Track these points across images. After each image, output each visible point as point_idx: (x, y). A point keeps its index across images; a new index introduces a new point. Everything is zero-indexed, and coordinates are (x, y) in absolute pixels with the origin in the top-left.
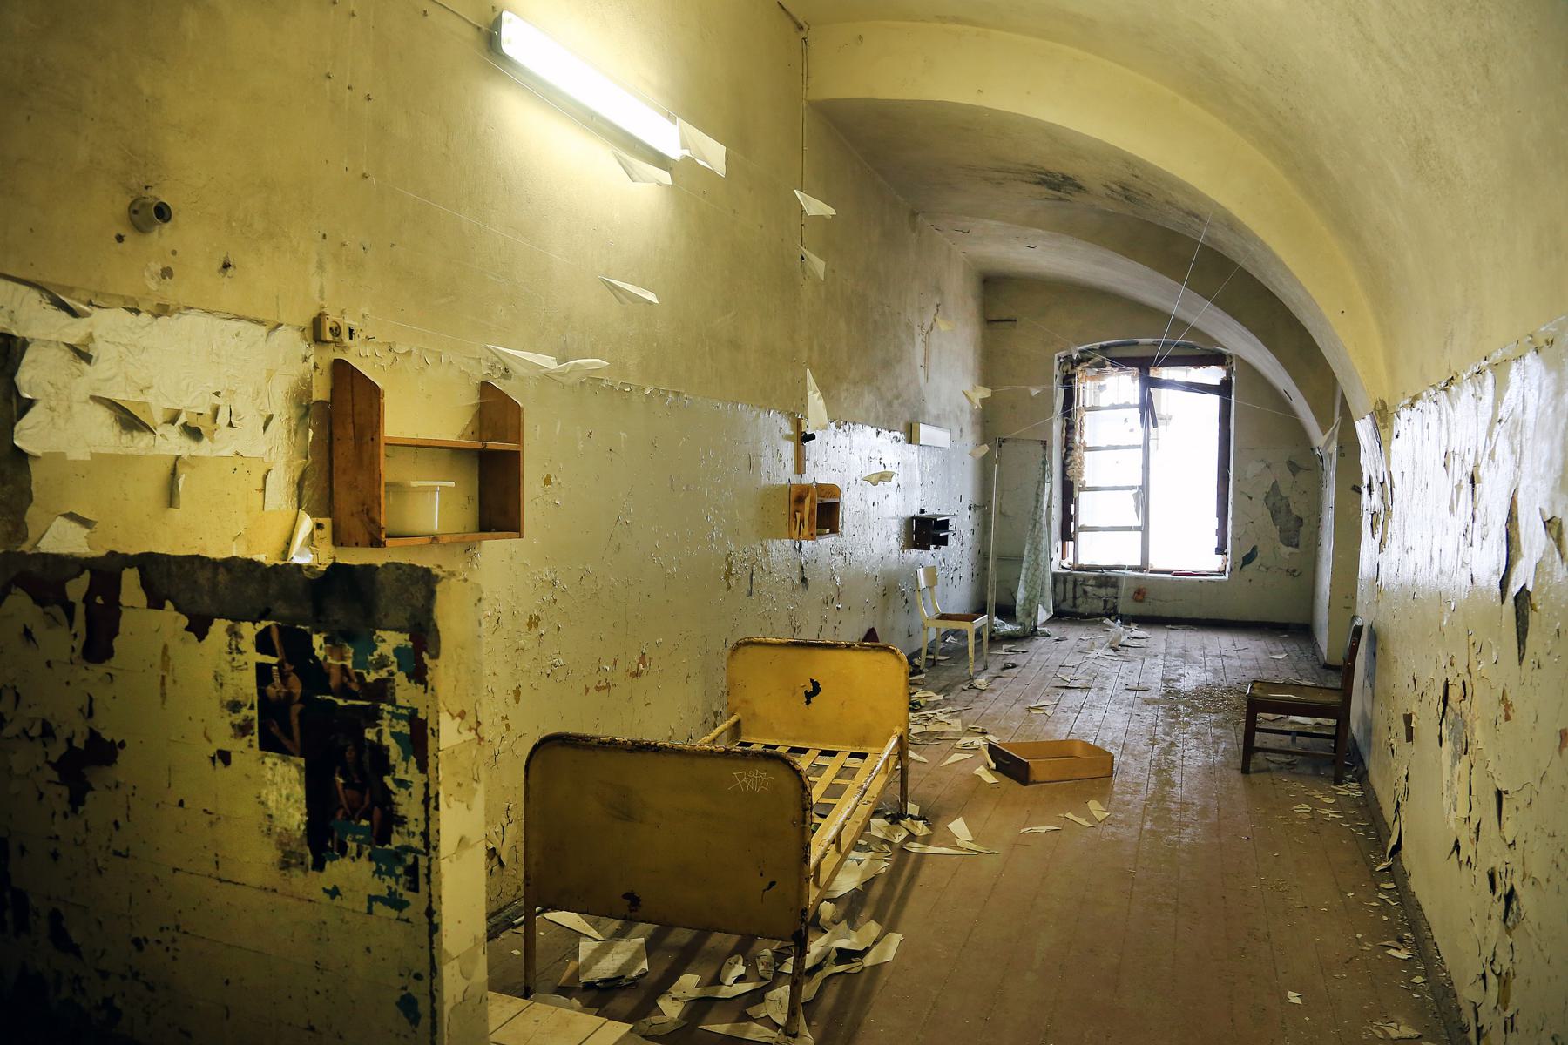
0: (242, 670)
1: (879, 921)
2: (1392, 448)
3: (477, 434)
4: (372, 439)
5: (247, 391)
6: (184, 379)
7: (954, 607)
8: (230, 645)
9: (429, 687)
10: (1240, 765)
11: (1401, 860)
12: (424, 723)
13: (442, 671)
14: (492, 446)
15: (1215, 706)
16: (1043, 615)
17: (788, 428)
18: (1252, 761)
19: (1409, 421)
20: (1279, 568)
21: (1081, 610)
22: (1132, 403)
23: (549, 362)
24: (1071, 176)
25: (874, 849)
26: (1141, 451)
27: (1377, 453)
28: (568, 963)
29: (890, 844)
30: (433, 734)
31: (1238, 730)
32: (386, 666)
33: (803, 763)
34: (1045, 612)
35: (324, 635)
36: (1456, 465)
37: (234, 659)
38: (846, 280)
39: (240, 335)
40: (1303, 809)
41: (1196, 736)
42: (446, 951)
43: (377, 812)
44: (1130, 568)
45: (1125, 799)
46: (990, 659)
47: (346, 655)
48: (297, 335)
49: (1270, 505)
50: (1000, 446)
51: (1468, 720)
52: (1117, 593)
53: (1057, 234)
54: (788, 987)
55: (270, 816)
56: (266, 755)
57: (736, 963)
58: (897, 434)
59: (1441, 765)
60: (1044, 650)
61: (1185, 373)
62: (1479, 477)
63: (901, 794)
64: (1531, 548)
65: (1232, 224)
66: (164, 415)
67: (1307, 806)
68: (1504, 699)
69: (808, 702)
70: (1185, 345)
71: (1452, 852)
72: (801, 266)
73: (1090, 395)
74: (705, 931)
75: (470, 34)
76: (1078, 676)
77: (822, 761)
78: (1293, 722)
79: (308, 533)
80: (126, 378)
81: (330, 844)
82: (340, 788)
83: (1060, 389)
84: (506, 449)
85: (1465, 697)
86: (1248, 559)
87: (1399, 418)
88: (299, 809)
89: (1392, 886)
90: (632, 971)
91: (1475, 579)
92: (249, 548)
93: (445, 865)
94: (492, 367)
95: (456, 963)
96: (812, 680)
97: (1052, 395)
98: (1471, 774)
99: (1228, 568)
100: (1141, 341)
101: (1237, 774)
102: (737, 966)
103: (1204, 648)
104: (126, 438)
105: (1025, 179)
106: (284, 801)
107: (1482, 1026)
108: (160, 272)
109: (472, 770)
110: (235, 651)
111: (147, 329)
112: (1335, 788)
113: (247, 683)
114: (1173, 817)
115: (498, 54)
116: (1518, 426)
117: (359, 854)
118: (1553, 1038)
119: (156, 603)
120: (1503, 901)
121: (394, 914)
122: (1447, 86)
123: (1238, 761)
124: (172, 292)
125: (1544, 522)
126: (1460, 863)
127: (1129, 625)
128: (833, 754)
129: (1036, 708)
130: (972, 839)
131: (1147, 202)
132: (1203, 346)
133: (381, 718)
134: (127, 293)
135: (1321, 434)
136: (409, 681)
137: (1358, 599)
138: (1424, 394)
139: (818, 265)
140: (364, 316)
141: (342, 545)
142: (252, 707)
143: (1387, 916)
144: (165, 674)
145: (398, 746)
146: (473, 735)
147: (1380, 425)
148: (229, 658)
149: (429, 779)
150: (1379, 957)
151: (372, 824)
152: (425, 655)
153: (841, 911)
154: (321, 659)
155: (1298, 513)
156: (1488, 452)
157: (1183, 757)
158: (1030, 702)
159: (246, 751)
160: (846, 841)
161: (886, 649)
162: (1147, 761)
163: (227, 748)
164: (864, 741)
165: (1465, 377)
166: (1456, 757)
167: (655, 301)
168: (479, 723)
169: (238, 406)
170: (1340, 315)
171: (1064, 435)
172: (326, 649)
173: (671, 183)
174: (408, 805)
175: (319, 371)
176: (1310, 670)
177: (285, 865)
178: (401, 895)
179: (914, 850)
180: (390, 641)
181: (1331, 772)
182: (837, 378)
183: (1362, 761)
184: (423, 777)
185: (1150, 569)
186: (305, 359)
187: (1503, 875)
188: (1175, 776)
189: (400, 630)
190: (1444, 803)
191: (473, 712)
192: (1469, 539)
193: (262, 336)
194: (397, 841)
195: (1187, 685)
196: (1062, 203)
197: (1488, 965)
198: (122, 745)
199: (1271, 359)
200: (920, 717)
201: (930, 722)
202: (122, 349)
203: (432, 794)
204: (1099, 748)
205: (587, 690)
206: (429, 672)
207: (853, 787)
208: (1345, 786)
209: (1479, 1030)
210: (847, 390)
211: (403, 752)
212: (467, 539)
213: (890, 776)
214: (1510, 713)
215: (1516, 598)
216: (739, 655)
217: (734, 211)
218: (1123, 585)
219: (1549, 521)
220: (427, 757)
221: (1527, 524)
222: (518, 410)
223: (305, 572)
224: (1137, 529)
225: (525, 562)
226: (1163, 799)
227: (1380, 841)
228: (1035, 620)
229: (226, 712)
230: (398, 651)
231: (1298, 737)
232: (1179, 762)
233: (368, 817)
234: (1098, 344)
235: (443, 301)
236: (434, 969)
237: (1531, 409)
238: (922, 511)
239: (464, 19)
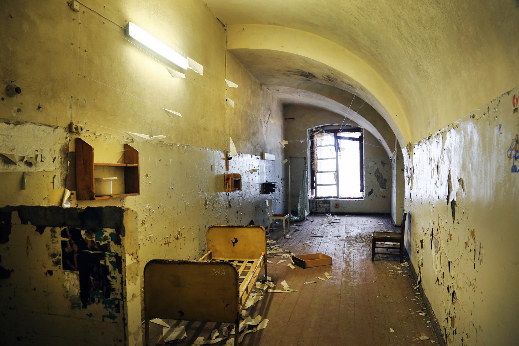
0: (56, 243)
1: (261, 315)
2: (413, 157)
3: (123, 161)
4: (90, 164)
5: (47, 149)
6: (26, 146)
7: (278, 212)
8: (52, 235)
9: (122, 246)
10: (371, 259)
11: (421, 286)
12: (121, 257)
13: (126, 241)
14: (129, 165)
15: (362, 240)
16: (306, 214)
17: (223, 156)
18: (375, 257)
19: (418, 149)
20: (380, 196)
21: (318, 211)
22: (332, 144)
23: (147, 137)
24: (311, 73)
25: (257, 292)
26: (335, 159)
27: (409, 159)
28: (160, 336)
29: (262, 290)
30: (124, 261)
31: (370, 247)
32: (107, 240)
33: (235, 264)
34: (307, 213)
35: (85, 231)
36: (432, 163)
37: (53, 240)
38: (240, 107)
39: (45, 131)
40: (391, 271)
41: (357, 250)
42: (129, 332)
43: (105, 288)
44: (333, 197)
45: (336, 271)
46: (290, 229)
47: (93, 237)
48: (63, 130)
49: (376, 176)
50: (291, 159)
51: (439, 241)
52: (330, 206)
53: (307, 91)
54: (233, 339)
55: (67, 291)
56: (66, 271)
57: (216, 332)
58: (258, 156)
59: (432, 255)
60: (307, 225)
61: (348, 134)
62: (439, 166)
63: (265, 274)
64: (455, 188)
65: (362, 89)
66: (19, 158)
67: (392, 270)
68: (449, 234)
69: (234, 245)
70: (348, 125)
71: (436, 282)
72: (226, 103)
73: (319, 142)
74: (204, 322)
75: (118, 29)
76: (319, 233)
77: (239, 264)
78: (386, 244)
79: (69, 197)
80: (6, 146)
81: (88, 299)
82: (92, 280)
83: (309, 141)
84: (134, 166)
85: (438, 234)
86: (370, 193)
87: (415, 148)
88: (77, 288)
89: (419, 293)
90: (181, 337)
91: (439, 198)
92: (49, 202)
93: (128, 303)
94: (128, 139)
95: (132, 336)
96: (235, 238)
97: (307, 143)
98: (441, 257)
99: (364, 196)
100: (334, 124)
101: (370, 262)
102: (216, 333)
103: (358, 222)
104: (6, 167)
105: (297, 74)
106: (72, 286)
107: (447, 334)
108: (17, 110)
109: (136, 272)
110: (54, 237)
111: (13, 129)
112: (401, 264)
113: (59, 247)
114: (352, 276)
115: (128, 36)
116: (449, 151)
117: (99, 302)
118: (467, 334)
119: (24, 222)
120: (452, 295)
121: (111, 321)
122: (425, 49)
123: (370, 257)
124: (22, 117)
125: (458, 180)
126: (439, 285)
127: (334, 216)
128: (242, 262)
129: (306, 244)
130: (289, 287)
131: (336, 81)
132: (353, 126)
133: (106, 257)
134: (6, 117)
135: (391, 153)
136: (115, 244)
137: (405, 205)
138: (422, 141)
139: (232, 103)
140: (85, 123)
141: (80, 200)
142: (60, 255)
143: (418, 303)
144: (28, 246)
145: (112, 266)
146: (136, 261)
147: (409, 150)
148: (52, 240)
149: (122, 276)
150: (416, 316)
151: (103, 292)
152: (120, 236)
153: (248, 313)
154: (84, 238)
155: (385, 178)
156: (441, 159)
157: (353, 257)
158: (304, 242)
159: (58, 271)
160: (249, 290)
161: (258, 227)
162: (342, 259)
163: (51, 269)
164: (252, 257)
165: (434, 136)
166: (436, 252)
167: (181, 116)
168: (137, 257)
169: (44, 155)
170: (396, 117)
171: (311, 155)
172: (86, 235)
173: (185, 78)
174: (116, 285)
175: (71, 142)
176: (391, 227)
177: (73, 307)
178: (114, 314)
179: (270, 292)
180: (108, 232)
181: (399, 260)
182: (238, 139)
183: (408, 255)
184: (121, 275)
185: (340, 197)
186: (66, 138)
187: (451, 287)
188: (351, 264)
189: (112, 228)
190: (433, 266)
191: (136, 253)
192: (437, 185)
193: (52, 131)
194: (112, 296)
195: (353, 234)
196: (309, 81)
197: (448, 315)
198: (12, 271)
199: (375, 130)
200: (269, 248)
201: (272, 250)
202: (4, 136)
203: (124, 280)
204: (327, 256)
205: (161, 244)
206: (122, 241)
207: (250, 272)
208: (403, 263)
209: (446, 335)
210: (242, 143)
211: (114, 267)
212: (122, 196)
213: (261, 268)
214: (451, 238)
215: (452, 203)
216: (210, 231)
217: (204, 86)
218: (332, 203)
219: (460, 179)
220: (122, 268)
221: (453, 181)
222: (137, 153)
223: (78, 210)
224: (335, 184)
225: (140, 203)
226: (348, 271)
227: (415, 280)
228: (304, 215)
229: (51, 258)
230: (111, 235)
231: (388, 249)
232: (352, 259)
233: (102, 289)
234: (321, 126)
235: (112, 117)
236: (126, 338)
237: (453, 146)
238: (267, 181)
239: (116, 24)
